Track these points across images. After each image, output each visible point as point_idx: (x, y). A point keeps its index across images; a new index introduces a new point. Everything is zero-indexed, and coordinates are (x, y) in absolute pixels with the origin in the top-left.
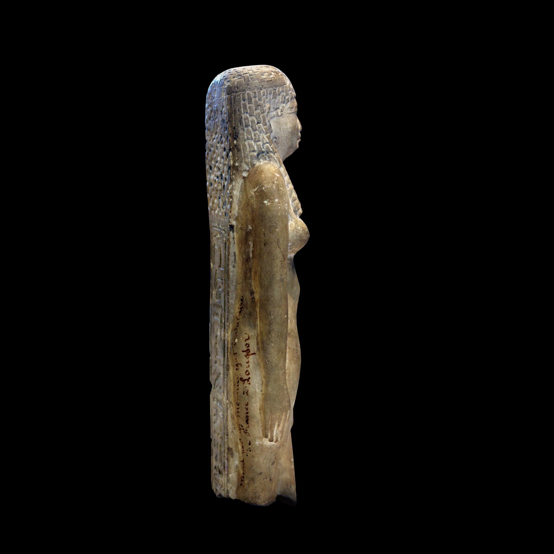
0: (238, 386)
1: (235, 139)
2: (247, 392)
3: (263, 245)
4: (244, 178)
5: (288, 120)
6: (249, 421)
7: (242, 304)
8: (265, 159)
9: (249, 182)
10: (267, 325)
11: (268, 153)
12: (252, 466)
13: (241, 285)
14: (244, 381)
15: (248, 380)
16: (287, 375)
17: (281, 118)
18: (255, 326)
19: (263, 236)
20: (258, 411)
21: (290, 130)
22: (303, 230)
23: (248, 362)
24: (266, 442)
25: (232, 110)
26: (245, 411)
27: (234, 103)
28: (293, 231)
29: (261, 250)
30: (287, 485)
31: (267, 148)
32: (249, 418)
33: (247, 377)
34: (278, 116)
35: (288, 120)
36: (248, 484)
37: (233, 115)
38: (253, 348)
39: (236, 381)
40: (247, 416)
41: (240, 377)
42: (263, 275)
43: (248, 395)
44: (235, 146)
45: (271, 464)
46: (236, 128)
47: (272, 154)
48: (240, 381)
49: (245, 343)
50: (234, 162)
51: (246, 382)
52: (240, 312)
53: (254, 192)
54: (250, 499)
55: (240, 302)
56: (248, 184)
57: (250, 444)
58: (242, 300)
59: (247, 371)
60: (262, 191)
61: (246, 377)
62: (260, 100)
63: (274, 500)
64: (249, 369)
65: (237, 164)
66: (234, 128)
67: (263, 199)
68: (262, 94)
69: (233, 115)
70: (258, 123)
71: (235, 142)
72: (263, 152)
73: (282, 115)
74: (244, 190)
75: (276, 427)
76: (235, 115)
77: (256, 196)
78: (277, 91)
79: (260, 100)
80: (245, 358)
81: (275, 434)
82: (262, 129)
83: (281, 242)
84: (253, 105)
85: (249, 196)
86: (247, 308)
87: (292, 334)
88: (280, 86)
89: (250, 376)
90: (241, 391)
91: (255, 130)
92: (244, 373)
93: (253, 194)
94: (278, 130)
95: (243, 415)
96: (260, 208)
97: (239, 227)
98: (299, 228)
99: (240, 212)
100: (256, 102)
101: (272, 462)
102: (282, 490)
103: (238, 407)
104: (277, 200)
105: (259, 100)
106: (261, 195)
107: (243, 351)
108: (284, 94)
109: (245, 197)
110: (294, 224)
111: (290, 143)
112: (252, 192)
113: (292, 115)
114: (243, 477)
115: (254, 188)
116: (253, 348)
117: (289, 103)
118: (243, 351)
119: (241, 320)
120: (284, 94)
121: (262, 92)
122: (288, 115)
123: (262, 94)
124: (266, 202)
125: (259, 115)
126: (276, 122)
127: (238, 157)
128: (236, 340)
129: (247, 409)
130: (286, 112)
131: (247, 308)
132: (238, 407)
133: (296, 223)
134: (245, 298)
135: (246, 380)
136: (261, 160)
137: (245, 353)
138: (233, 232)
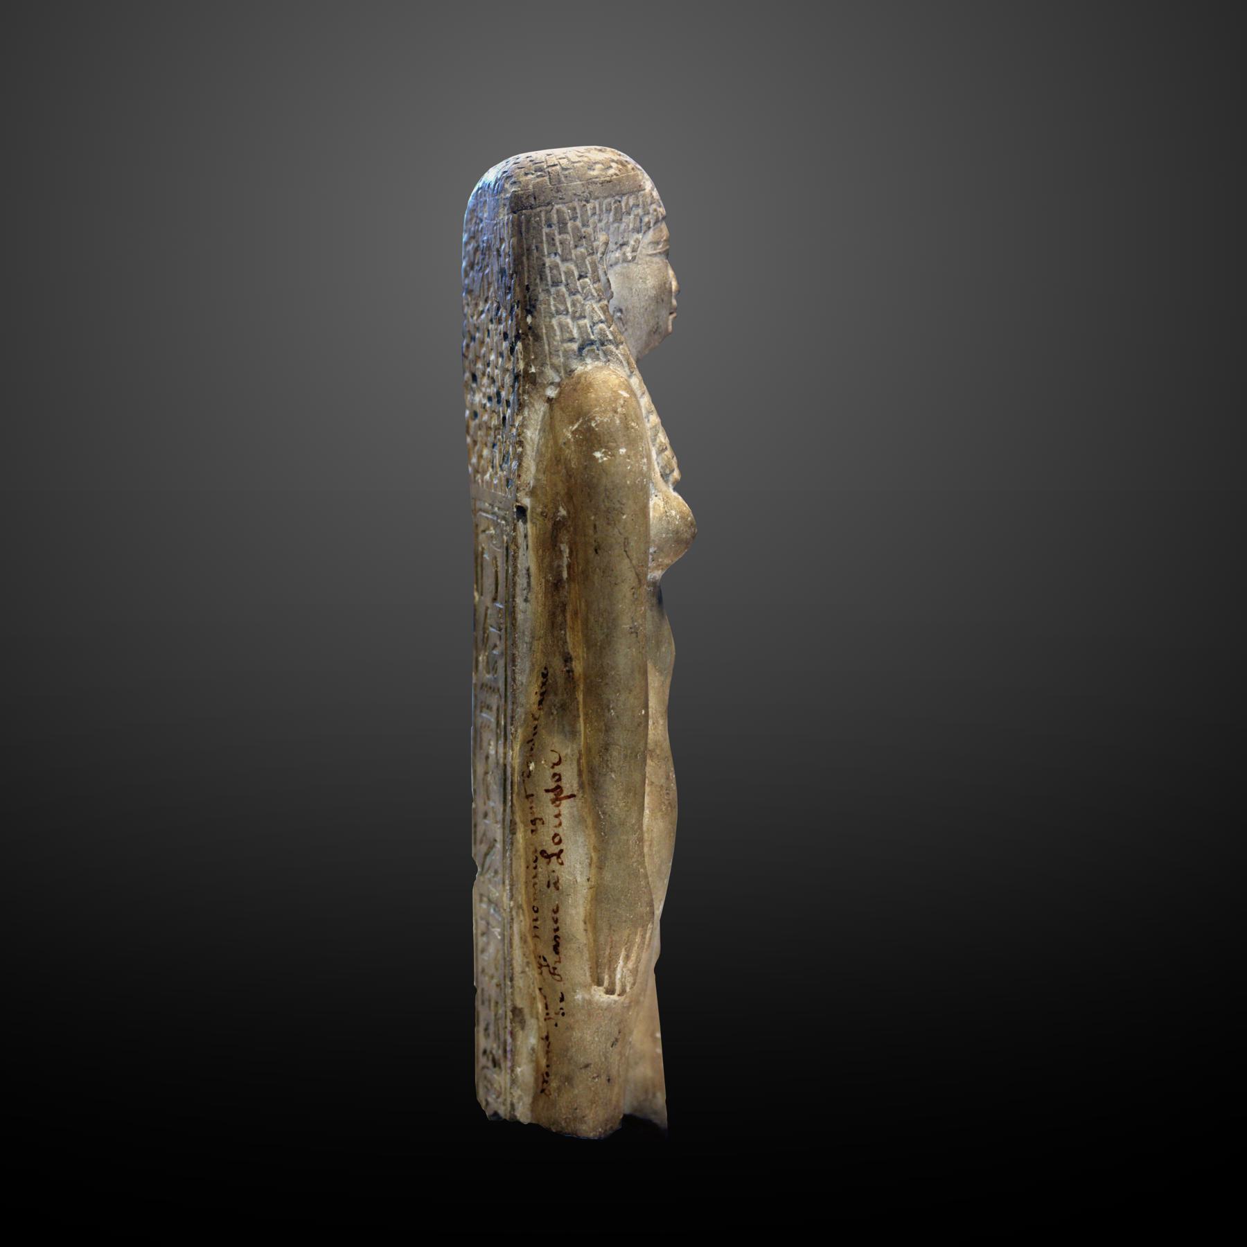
0: (535, 868)
1: (529, 312)
2: (556, 883)
3: (591, 551)
4: (549, 400)
5: (648, 271)
6: (560, 949)
7: (544, 684)
8: (597, 358)
9: (562, 409)
10: (600, 730)
11: (603, 344)
12: (567, 1050)
13: (542, 641)
14: (549, 857)
15: (558, 855)
16: (647, 843)
17: (632, 265)
18: (574, 733)
19: (591, 532)
20: (581, 926)
21: (653, 293)
22: (682, 518)
23: (557, 816)
24: (599, 995)
25: (522, 247)
26: (550, 925)
27: (528, 231)
28: (661, 519)
29: (587, 562)
30: (646, 1092)
31: (602, 332)
32: (562, 942)
33: (555, 849)
34: (625, 260)
35: (648, 271)
36: (559, 1089)
37: (525, 259)
38: (570, 782)
39: (532, 858)
40: (556, 937)
41: (540, 849)
42: (592, 618)
43: (558, 889)
44: (530, 328)
45: (609, 1044)
46: (531, 288)
47: (612, 347)
48: (539, 857)
49: (552, 771)
50: (528, 365)
51: (554, 859)
52: (540, 703)
53: (573, 433)
54: (563, 1124)
55: (541, 679)
56: (558, 413)
57: (562, 1000)
58: (545, 676)
59: (556, 835)
60: (590, 429)
61: (553, 849)
62: (585, 225)
63: (617, 1126)
64: (560, 831)
65: (533, 370)
66: (528, 288)
67: (592, 449)
68: (589, 213)
69: (525, 259)
70: (581, 277)
71: (529, 320)
72: (592, 343)
73: (634, 258)
74: (549, 427)
75: (621, 962)
76: (528, 259)
77: (577, 442)
78: (623, 204)
79: (585, 225)
80: (551, 806)
81: (618, 976)
82: (590, 291)
83: (632, 544)
84: (569, 237)
85: (561, 441)
86: (556, 694)
87: (658, 752)
88: (631, 193)
89: (562, 846)
90: (542, 879)
91: (573, 293)
92: (548, 839)
93: (570, 436)
94: (625, 293)
95: (547, 934)
96: (586, 467)
97: (539, 510)
98: (674, 513)
99: (541, 476)
100: (576, 229)
101: (613, 1039)
102: (635, 1104)
103: (535, 915)
104: (623, 451)
105: (584, 225)
106: (587, 440)
107: (547, 791)
108: (640, 211)
109: (551, 443)
110: (662, 504)
111: (652, 323)
112: (568, 433)
113: (657, 259)
114: (547, 1074)
115: (572, 424)
116: (570, 782)
117: (651, 232)
118: (547, 791)
119: (542, 721)
120: (640, 211)
121: (589, 206)
122: (648, 259)
123: (589, 213)
124: (598, 455)
125: (584, 258)
126: (622, 274)
127: (535, 354)
128: (532, 766)
129: (556, 921)
130: (644, 252)
131: (556, 694)
132: (535, 915)
133: (666, 503)
134: (551, 671)
135: (553, 855)
136: (589, 361)
137: (552, 795)
138: (525, 522)
